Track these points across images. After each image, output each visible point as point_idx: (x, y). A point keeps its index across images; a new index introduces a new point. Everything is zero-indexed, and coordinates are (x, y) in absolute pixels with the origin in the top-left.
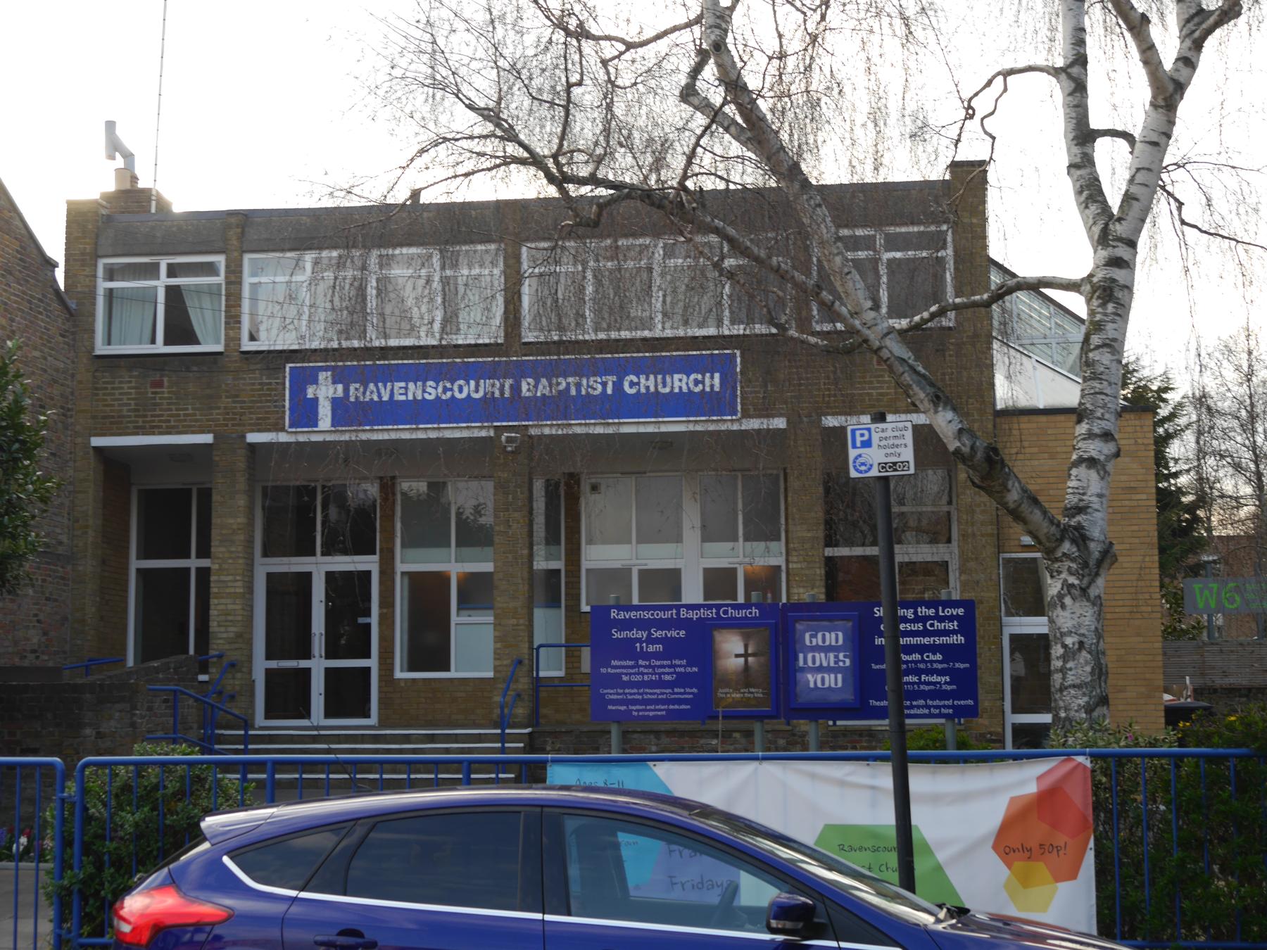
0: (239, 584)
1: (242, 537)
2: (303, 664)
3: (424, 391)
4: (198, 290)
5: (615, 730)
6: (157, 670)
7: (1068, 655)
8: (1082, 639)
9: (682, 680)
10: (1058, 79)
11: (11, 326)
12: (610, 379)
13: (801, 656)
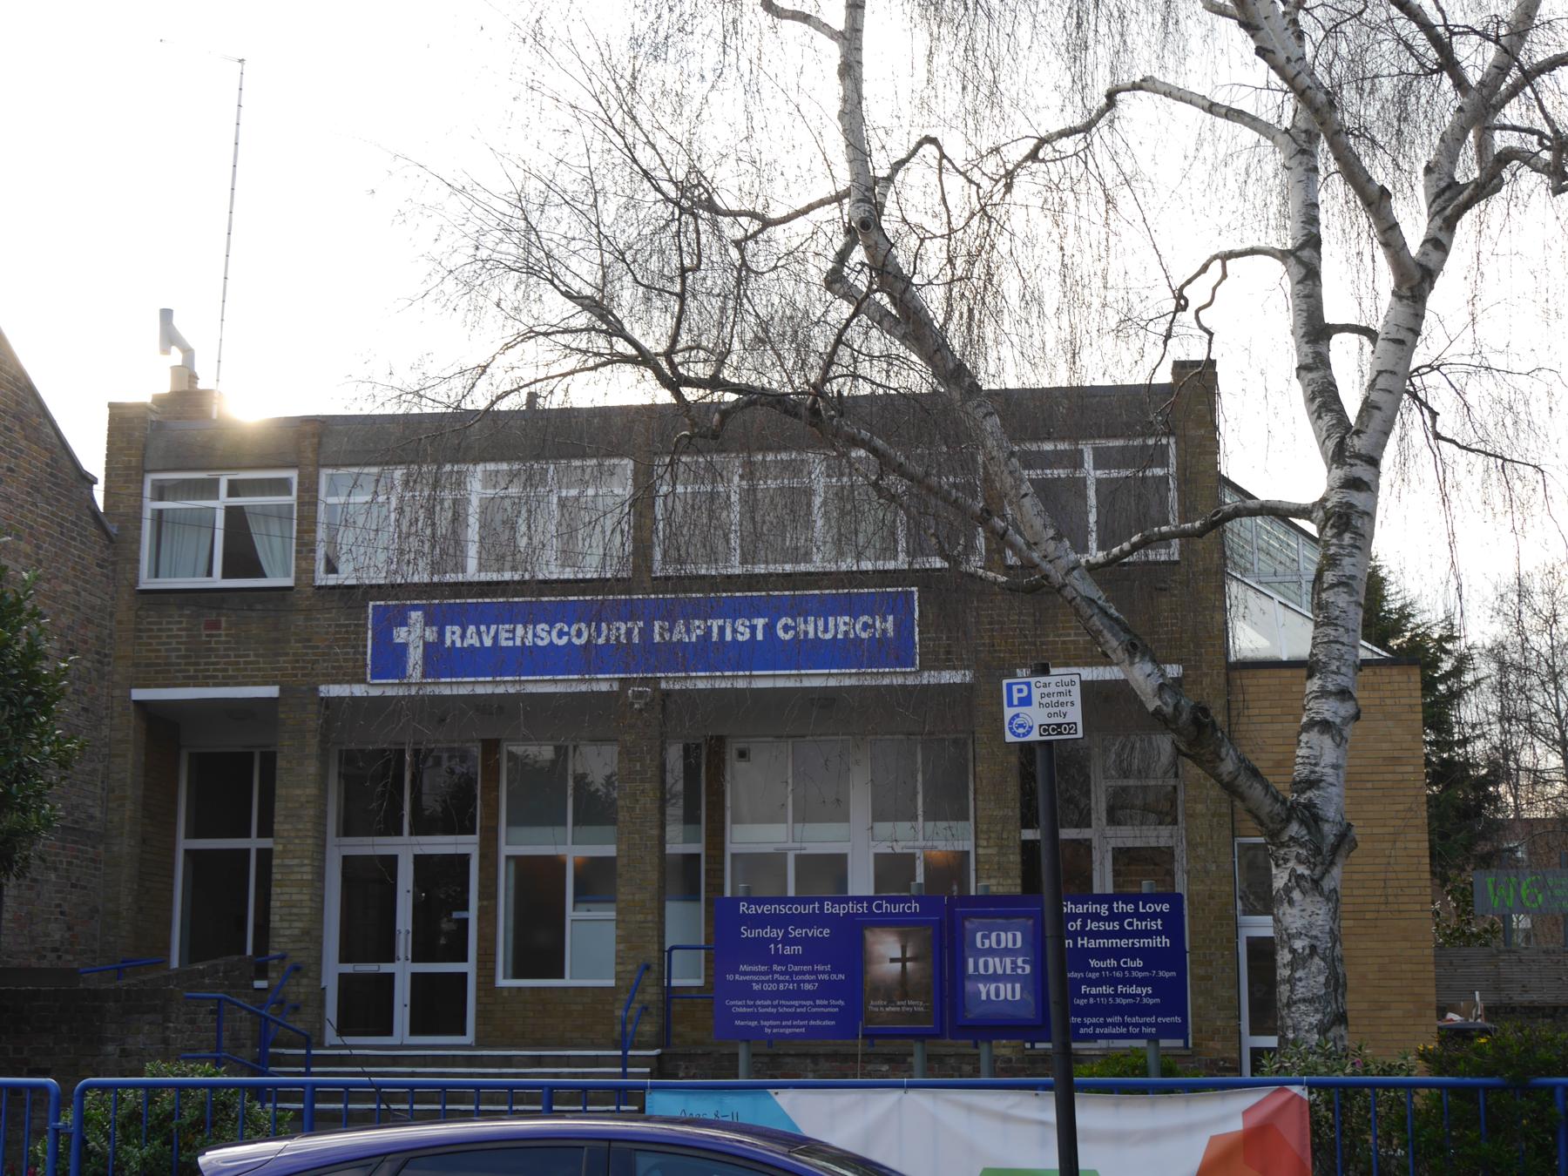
0: (308, 869)
1: (312, 812)
2: (385, 968)
3: (535, 635)
4: (266, 513)
5: (743, 1052)
6: (202, 974)
7: (1298, 961)
8: (1314, 942)
9: (827, 990)
10: (1284, 263)
11: (38, 554)
12: (760, 622)
13: (971, 961)
